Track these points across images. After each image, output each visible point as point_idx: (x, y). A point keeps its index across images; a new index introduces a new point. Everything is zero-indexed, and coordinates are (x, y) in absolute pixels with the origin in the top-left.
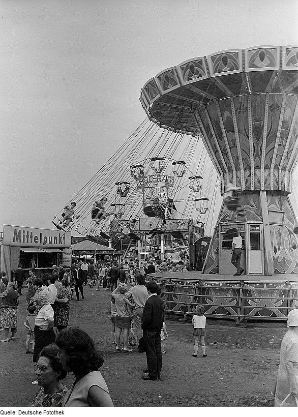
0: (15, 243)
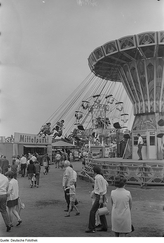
0: (21, 142)
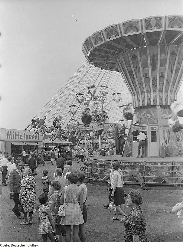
0: (8, 139)
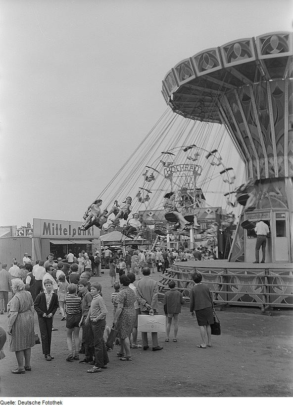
0: (45, 236)
